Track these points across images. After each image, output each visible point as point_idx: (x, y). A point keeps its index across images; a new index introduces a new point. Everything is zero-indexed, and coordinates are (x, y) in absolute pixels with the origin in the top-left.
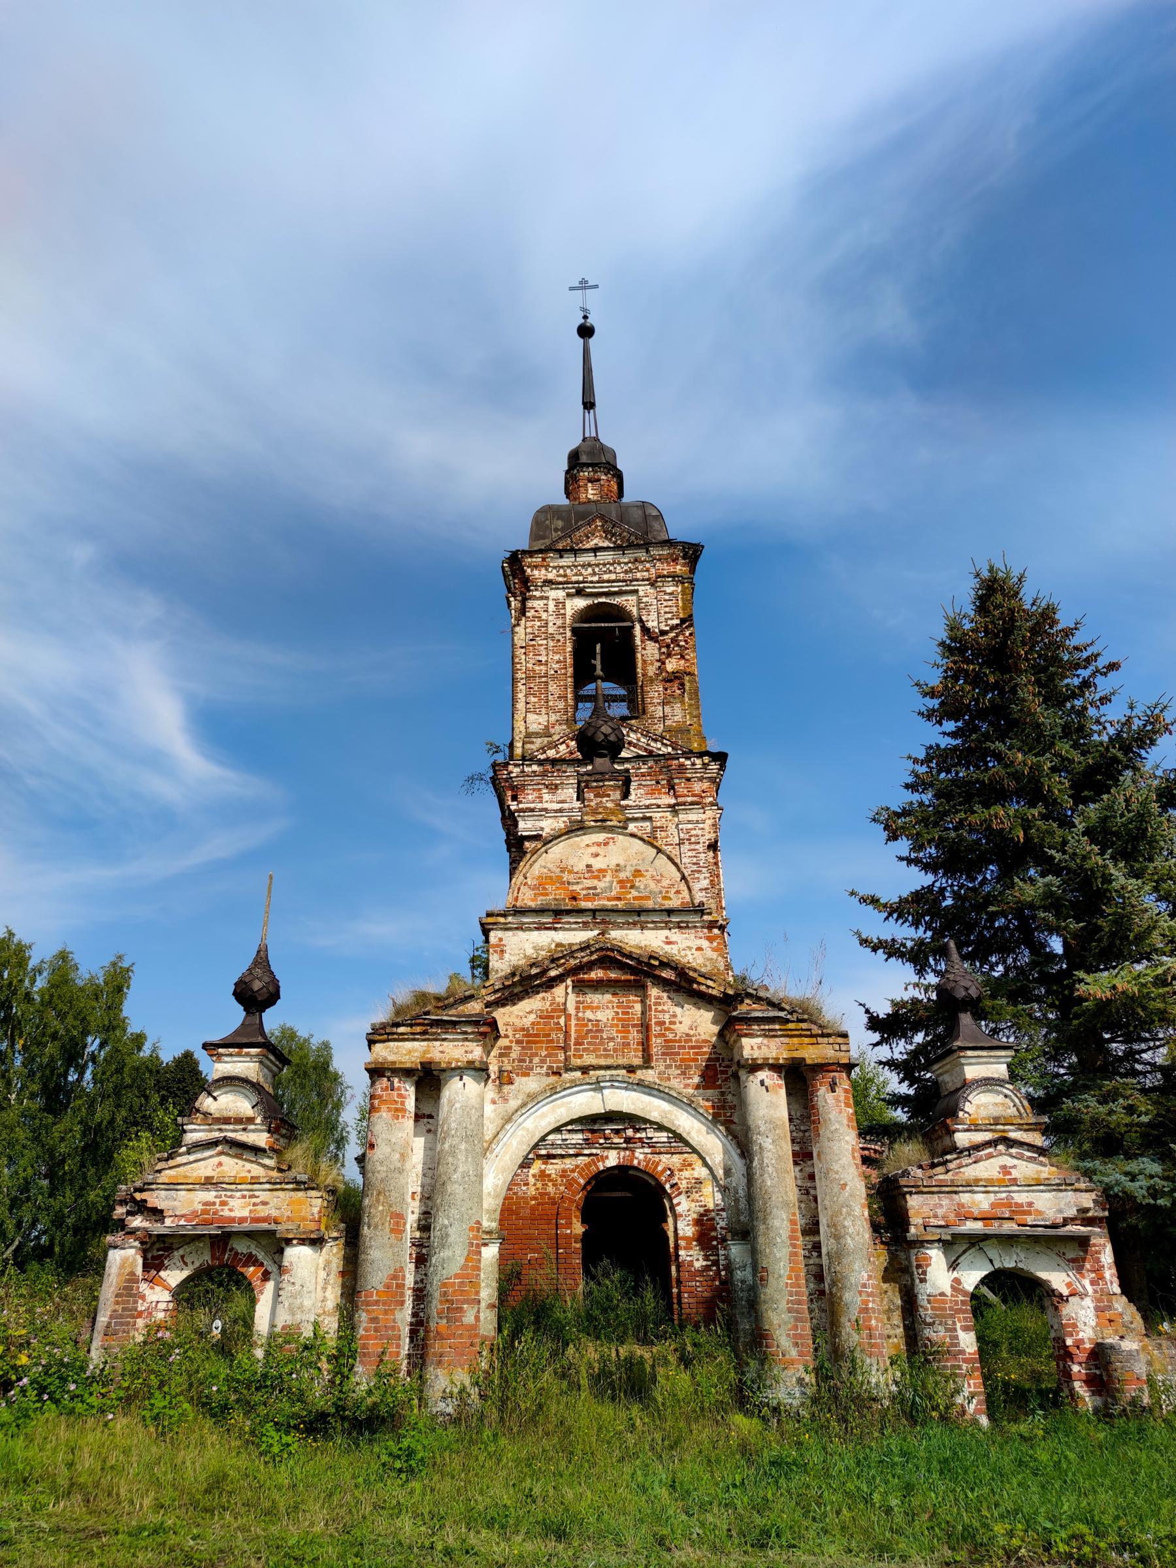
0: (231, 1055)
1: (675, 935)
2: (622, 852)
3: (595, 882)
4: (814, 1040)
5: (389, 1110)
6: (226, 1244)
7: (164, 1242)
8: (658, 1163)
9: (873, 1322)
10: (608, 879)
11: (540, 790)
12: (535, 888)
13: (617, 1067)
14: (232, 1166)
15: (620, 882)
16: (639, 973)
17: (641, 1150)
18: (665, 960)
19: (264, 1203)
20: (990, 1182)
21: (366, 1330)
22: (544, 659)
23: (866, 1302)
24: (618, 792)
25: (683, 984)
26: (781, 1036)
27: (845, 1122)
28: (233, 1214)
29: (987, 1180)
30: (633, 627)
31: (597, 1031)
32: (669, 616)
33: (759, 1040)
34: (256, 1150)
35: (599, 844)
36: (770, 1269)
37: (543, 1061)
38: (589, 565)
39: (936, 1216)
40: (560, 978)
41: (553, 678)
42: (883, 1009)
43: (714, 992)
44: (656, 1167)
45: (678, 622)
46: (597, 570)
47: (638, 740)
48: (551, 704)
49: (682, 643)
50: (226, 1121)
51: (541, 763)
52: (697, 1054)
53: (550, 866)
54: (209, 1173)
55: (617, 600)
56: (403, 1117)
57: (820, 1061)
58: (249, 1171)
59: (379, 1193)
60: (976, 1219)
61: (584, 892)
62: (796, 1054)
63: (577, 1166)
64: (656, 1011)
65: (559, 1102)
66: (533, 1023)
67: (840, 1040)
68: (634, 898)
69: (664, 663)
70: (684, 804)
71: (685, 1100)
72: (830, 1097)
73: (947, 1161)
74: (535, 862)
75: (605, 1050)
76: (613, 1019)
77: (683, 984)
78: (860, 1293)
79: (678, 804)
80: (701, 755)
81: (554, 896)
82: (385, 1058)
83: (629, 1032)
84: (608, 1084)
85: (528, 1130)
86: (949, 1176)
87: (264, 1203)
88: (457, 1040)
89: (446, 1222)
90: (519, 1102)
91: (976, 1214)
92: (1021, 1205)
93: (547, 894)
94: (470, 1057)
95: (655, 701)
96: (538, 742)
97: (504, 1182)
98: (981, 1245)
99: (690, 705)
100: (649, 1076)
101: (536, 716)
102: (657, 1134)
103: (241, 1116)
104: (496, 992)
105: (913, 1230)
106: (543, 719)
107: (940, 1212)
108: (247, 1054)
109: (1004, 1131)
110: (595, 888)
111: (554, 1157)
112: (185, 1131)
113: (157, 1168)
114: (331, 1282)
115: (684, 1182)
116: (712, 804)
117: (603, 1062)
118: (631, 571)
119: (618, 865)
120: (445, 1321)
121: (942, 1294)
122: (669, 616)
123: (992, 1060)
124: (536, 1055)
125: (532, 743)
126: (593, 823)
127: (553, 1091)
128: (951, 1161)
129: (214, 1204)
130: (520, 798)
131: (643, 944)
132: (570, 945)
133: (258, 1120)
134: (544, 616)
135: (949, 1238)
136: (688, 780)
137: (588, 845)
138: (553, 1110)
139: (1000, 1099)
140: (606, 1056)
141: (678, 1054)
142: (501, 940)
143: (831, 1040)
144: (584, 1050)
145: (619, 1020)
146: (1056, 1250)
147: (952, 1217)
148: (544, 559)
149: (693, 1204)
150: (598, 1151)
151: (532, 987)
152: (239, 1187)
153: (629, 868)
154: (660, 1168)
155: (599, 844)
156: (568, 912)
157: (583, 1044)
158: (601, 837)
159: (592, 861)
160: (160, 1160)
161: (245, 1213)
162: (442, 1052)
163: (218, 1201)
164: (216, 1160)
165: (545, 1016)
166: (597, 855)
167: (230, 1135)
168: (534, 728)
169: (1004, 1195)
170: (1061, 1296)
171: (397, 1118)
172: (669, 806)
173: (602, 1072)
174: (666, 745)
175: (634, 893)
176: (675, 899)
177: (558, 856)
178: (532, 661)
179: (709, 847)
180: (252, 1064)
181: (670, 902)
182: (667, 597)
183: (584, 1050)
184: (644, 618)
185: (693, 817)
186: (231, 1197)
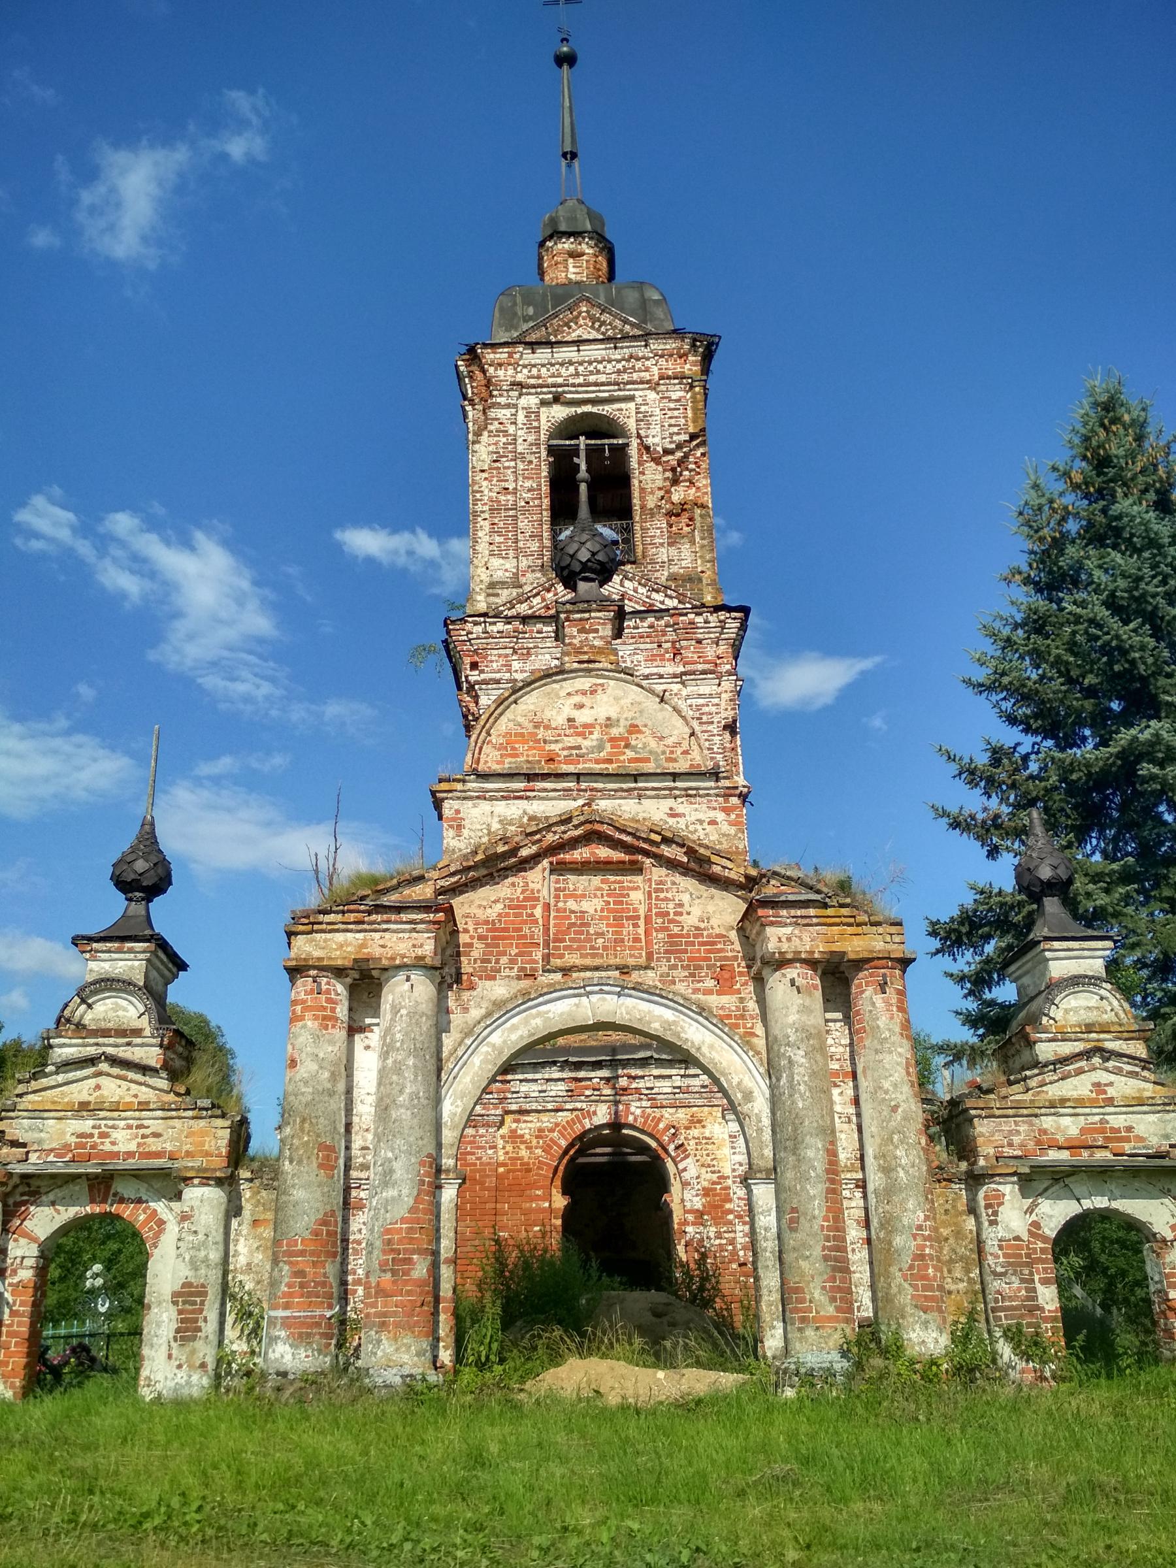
0: (109, 951)
1: (682, 806)
2: (612, 702)
3: (579, 740)
4: (859, 930)
5: (316, 1018)
6: (108, 1188)
7: (29, 1185)
8: (659, 1120)
9: (930, 1271)
10: (596, 736)
11: (507, 656)
12: (501, 747)
13: (607, 968)
14: (113, 1088)
15: (611, 740)
16: (635, 850)
17: (638, 1104)
18: (670, 835)
19: (156, 1135)
20: (1080, 1102)
21: (289, 1285)
22: (511, 486)
23: (923, 1247)
24: (609, 627)
25: (692, 865)
26: (817, 925)
27: (898, 1030)
28: (115, 1149)
29: (1076, 1100)
30: (627, 445)
31: (582, 925)
32: (675, 429)
33: (789, 930)
34: (144, 1069)
35: (584, 693)
36: (801, 1209)
37: (513, 961)
38: (571, 363)
39: (1010, 1145)
40: (535, 859)
41: (524, 511)
42: (947, 912)
43: (733, 875)
44: (657, 1124)
45: (687, 437)
46: (581, 368)
47: (635, 591)
48: (521, 544)
49: (692, 466)
50: (105, 1033)
51: (508, 620)
52: (709, 951)
53: (520, 719)
54: (85, 1097)
55: (606, 410)
56: (333, 1027)
57: (866, 955)
58: (136, 1096)
59: (304, 1120)
60: (1060, 1148)
61: (565, 753)
62: (836, 947)
63: (557, 1125)
64: (657, 898)
65: (534, 1011)
66: (500, 915)
67: (893, 929)
68: (630, 761)
69: (668, 492)
70: (693, 673)
71: (694, 1008)
72: (879, 999)
73: (1025, 1079)
74: (501, 714)
75: (592, 948)
76: (602, 910)
77: (692, 865)
78: (915, 1236)
79: (685, 673)
80: (717, 609)
81: (526, 757)
82: (309, 954)
83: (622, 926)
84: (597, 988)
85: (494, 1045)
86: (1028, 1097)
87: (156, 1135)
88: (403, 931)
89: (390, 1155)
90: (483, 1011)
91: (1061, 1140)
92: (1118, 1130)
93: (516, 756)
94: (420, 952)
95: (657, 541)
96: (505, 594)
97: (464, 1110)
98: (1067, 1181)
99: (702, 547)
100: (650, 978)
101: (501, 561)
102: (657, 1084)
103: (125, 1026)
104: (453, 874)
105: (982, 1162)
106: (510, 565)
107: (1016, 1140)
108: (131, 951)
109: (1098, 1040)
110: (579, 748)
111: (528, 1112)
112: (51, 1047)
113: (18, 1091)
114: (245, 1232)
115: (692, 1142)
116: (729, 673)
117: (588, 962)
118: (625, 370)
119: (608, 719)
120: (389, 1275)
121: (1017, 1238)
122: (675, 429)
123: (1086, 953)
124: (504, 953)
125: (497, 595)
126: (576, 665)
127: (526, 997)
128: (1030, 1078)
129: (91, 1136)
130: (482, 666)
131: (640, 817)
132: (547, 818)
133: (147, 1032)
134: (511, 429)
135: (1027, 1170)
136: (699, 642)
137: (569, 694)
138: (526, 1022)
139: (1094, 1001)
140: (594, 956)
141: (686, 951)
142: (458, 812)
143: (880, 930)
144: (565, 948)
145: (609, 911)
146: (1159, 1185)
147: (1031, 1145)
148: (511, 355)
149: (704, 1170)
150: (584, 1105)
151: (498, 871)
152: (123, 1114)
153: (622, 723)
154: (661, 1126)
155: (584, 693)
156: (545, 777)
157: (564, 940)
158: (585, 683)
159: (576, 714)
160: (20, 1082)
161: (132, 1147)
162: (383, 946)
163: (96, 1132)
164: (92, 1082)
165: (515, 906)
166: (580, 706)
167: (110, 1050)
168: (499, 575)
169: (1097, 1118)
170: (1164, 1241)
171: (326, 1028)
172: (675, 676)
173: (588, 974)
174: (671, 597)
175: (630, 754)
176: (681, 761)
177: (532, 707)
178: (496, 489)
179: (725, 727)
180: (137, 963)
181: (675, 765)
182: (672, 405)
183: (565, 948)
184: (642, 432)
185: (705, 689)
186: (113, 1127)
